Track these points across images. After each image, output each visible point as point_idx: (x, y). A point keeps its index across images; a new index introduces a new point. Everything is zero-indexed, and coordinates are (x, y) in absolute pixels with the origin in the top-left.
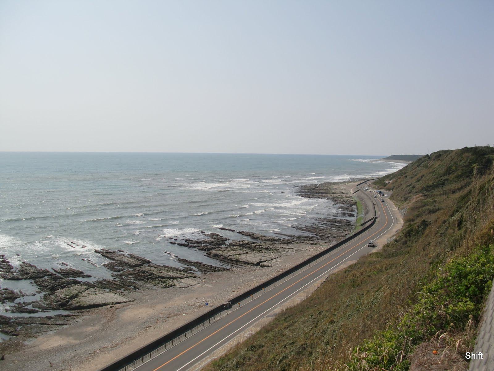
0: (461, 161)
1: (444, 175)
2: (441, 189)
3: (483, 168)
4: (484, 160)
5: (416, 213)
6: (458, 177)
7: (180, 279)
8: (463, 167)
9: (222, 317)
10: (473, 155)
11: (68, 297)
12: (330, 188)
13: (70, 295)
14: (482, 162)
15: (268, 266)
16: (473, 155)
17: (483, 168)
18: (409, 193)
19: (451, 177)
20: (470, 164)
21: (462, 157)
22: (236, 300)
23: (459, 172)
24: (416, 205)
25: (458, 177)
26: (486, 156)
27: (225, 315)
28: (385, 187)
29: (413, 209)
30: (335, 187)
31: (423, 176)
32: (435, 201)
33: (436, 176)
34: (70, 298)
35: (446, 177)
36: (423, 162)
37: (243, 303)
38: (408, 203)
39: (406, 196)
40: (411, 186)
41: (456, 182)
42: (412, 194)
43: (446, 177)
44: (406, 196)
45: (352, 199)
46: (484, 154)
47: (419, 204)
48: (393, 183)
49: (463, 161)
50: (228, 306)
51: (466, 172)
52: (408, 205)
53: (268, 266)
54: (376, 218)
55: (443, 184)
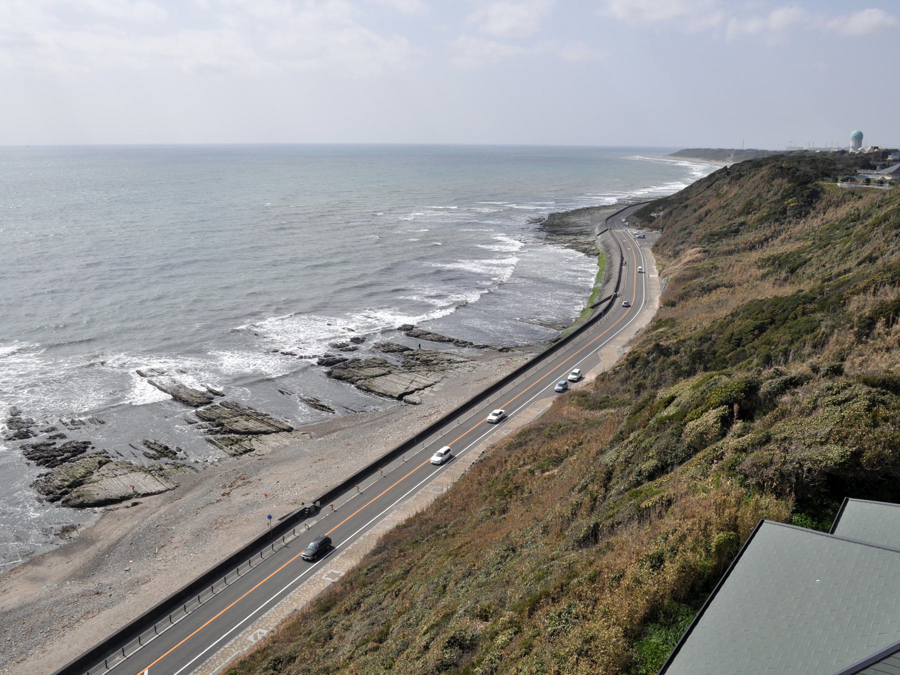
0: (769, 191)
1: (740, 214)
2: (732, 242)
3: (804, 206)
4: (806, 193)
5: (680, 290)
6: (761, 221)
7: (264, 436)
8: (772, 202)
9: (297, 534)
10: (789, 182)
11: (66, 483)
12: (563, 222)
13: (71, 480)
14: (803, 196)
15: (415, 404)
16: (789, 182)
17: (804, 206)
18: (683, 243)
19: (751, 218)
20: (783, 198)
21: (772, 185)
22: (327, 498)
23: (764, 212)
24: (684, 273)
25: (761, 221)
26: (810, 185)
27: (303, 530)
28: (651, 225)
29: (679, 280)
30: (573, 219)
31: (710, 211)
32: (716, 268)
33: (727, 216)
34: (69, 486)
35: (742, 219)
36: (717, 180)
37: (338, 503)
38: (676, 264)
39: (677, 248)
40: (687, 231)
41: (756, 229)
42: (686, 245)
43: (742, 219)
44: (677, 248)
45: (594, 248)
46: (807, 183)
47: (688, 273)
48: (664, 217)
49: (772, 193)
50: (313, 510)
51: (775, 213)
52: (676, 268)
53: (415, 404)
54: (616, 296)
55: (737, 231)
